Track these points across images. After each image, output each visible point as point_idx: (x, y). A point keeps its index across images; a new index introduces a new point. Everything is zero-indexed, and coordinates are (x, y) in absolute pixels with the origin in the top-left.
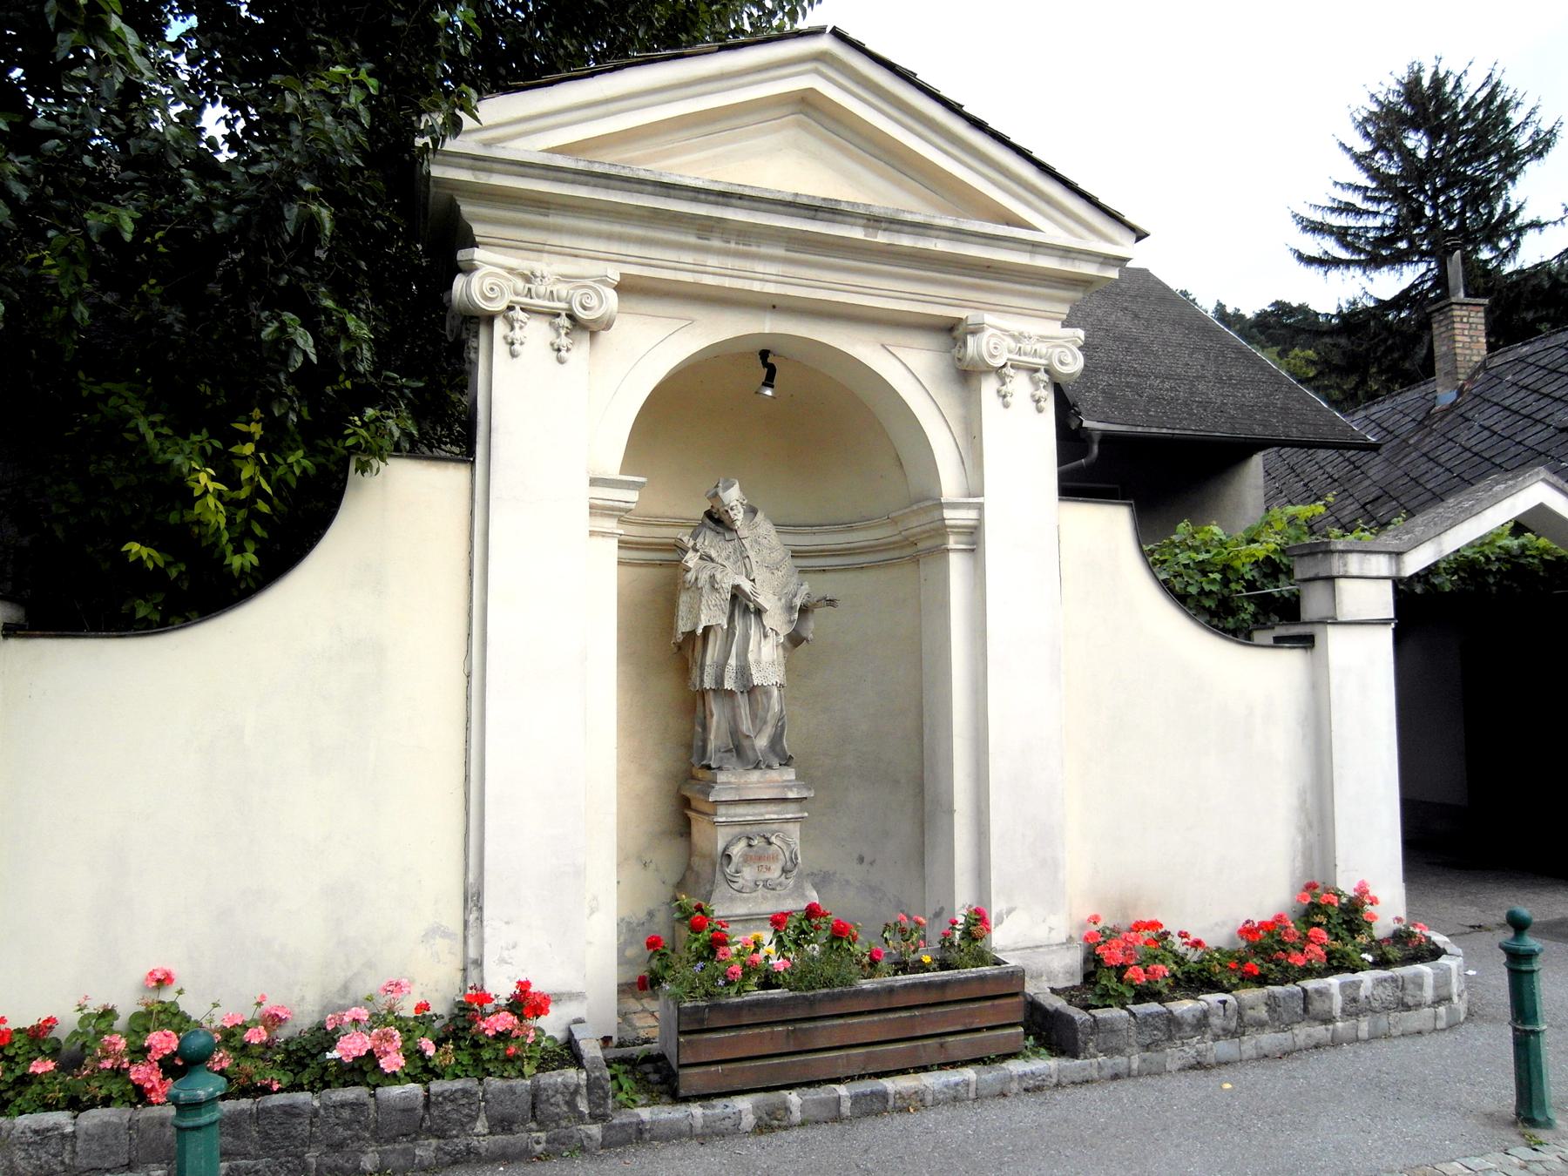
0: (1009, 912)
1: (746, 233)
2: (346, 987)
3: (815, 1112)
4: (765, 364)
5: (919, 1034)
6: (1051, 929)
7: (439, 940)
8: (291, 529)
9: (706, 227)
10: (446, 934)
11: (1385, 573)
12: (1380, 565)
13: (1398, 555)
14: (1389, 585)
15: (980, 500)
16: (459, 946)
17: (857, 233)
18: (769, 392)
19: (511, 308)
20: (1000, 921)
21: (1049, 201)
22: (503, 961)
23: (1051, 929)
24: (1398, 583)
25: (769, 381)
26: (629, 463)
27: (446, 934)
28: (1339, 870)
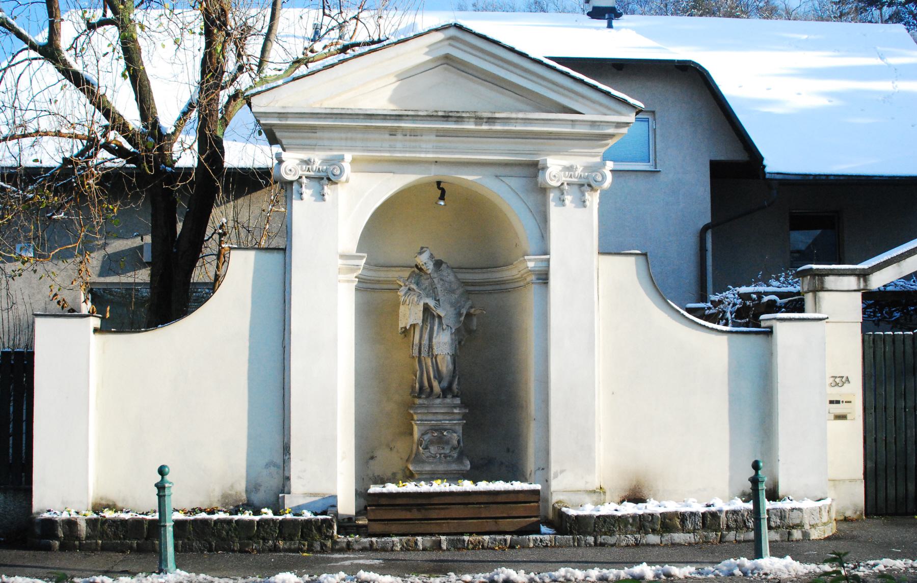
0: (562, 472)
1: (414, 133)
2: (232, 486)
3: (428, 545)
4: (439, 187)
5: (483, 516)
6: (587, 483)
7: (272, 468)
8: (864, 313)
9: (393, 132)
10: (275, 465)
11: (855, 288)
12: (851, 282)
13: (864, 275)
14: (859, 295)
15: (547, 257)
16: (281, 471)
17: (471, 126)
18: (442, 203)
19: (300, 177)
20: (556, 476)
21: (583, 97)
22: (299, 477)
23: (587, 483)
24: (867, 296)
25: (442, 197)
26: (359, 249)
27: (275, 465)
28: (780, 463)
